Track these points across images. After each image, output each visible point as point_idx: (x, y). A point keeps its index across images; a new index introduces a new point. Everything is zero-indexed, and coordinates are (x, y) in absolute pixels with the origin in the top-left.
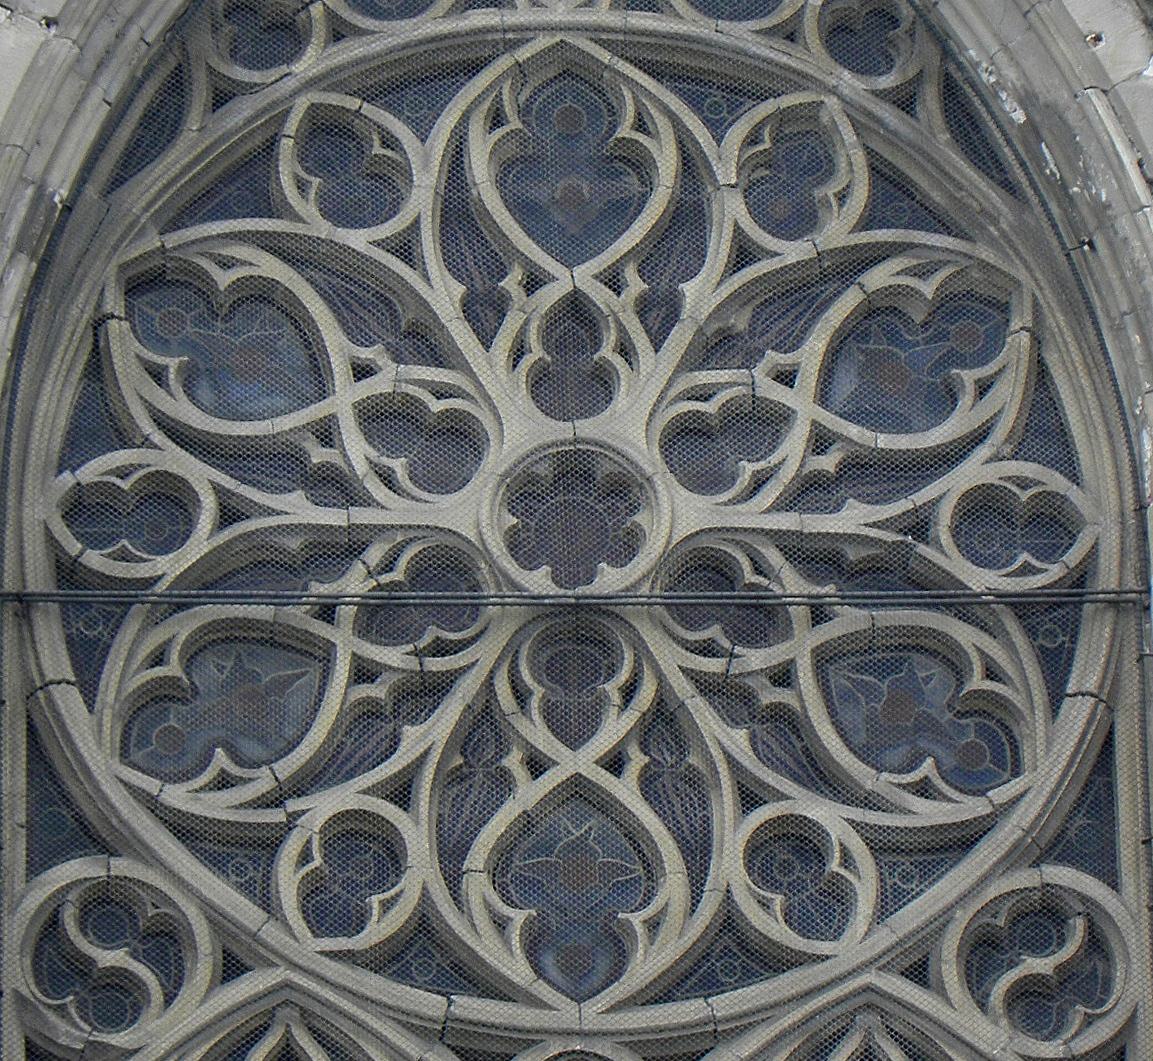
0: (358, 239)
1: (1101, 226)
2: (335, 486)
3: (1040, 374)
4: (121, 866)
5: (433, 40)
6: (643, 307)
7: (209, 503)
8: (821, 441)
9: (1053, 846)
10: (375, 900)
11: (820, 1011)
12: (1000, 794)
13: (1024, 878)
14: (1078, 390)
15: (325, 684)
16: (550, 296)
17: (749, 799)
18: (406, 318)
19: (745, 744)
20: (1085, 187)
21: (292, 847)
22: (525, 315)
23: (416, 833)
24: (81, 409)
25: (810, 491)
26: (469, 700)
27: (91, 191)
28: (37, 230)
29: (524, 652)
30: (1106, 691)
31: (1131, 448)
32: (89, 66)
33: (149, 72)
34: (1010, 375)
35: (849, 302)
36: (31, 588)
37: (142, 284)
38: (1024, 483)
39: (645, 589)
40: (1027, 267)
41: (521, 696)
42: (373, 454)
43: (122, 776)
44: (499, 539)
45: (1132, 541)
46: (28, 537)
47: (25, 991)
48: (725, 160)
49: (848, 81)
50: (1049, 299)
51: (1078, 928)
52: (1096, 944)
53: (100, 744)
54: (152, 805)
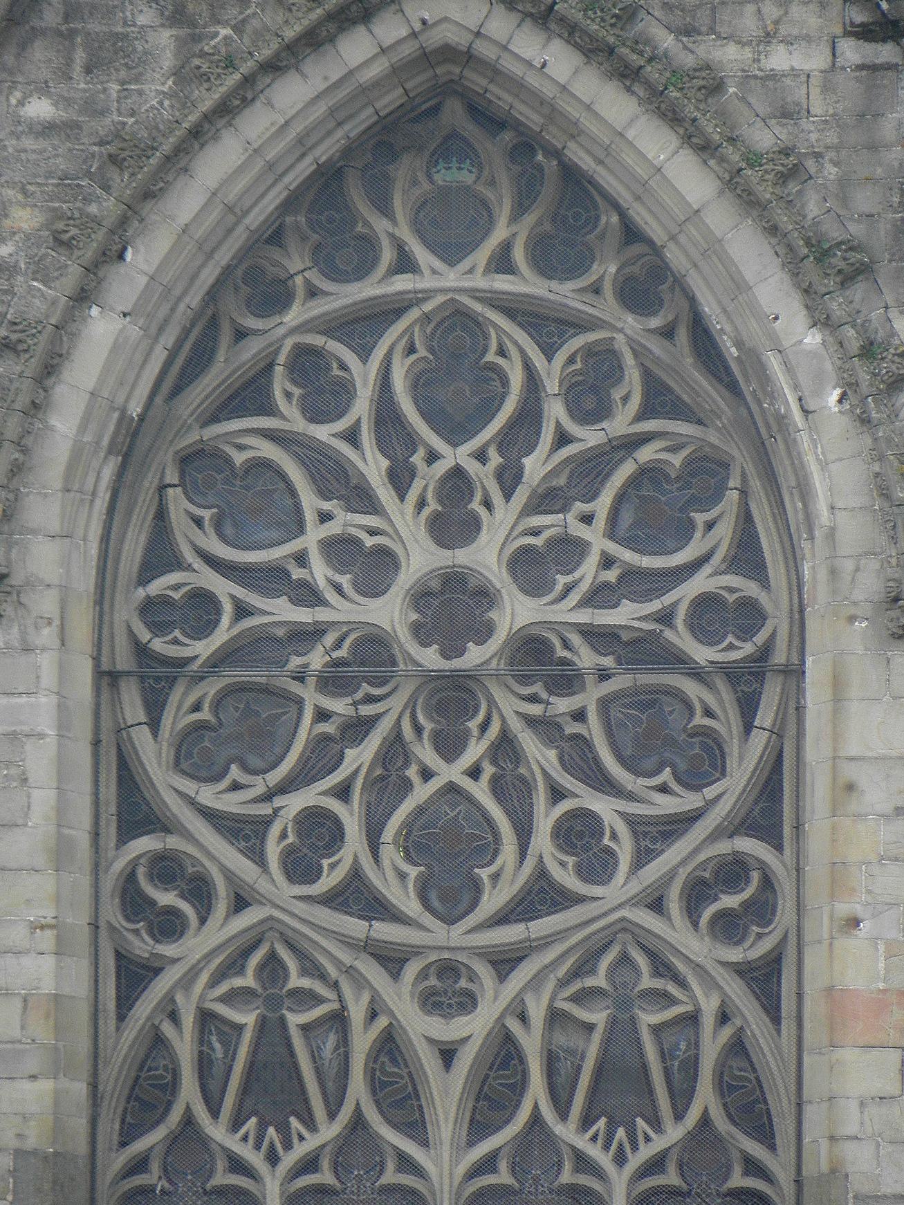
0: (322, 433)
1: (780, 430)
2: (307, 595)
3: (746, 518)
4: (173, 842)
5: (371, 299)
6: (500, 475)
7: (228, 608)
8: (607, 562)
9: (742, 824)
10: (325, 863)
11: (595, 933)
12: (710, 792)
13: (723, 847)
14: (767, 530)
15: (299, 722)
16: (441, 467)
17: (557, 794)
18: (354, 481)
19: (555, 761)
20: (771, 404)
21: (275, 830)
22: (428, 477)
23: (351, 820)
24: (150, 549)
25: (599, 596)
26: (384, 735)
27: (159, 400)
28: (120, 439)
29: (420, 701)
30: (777, 727)
31: (797, 571)
32: (153, 330)
33: (193, 325)
34: (726, 518)
35: (626, 470)
36: (119, 668)
37: (186, 460)
38: (731, 590)
39: (494, 664)
40: (739, 448)
41: (418, 730)
42: (330, 573)
43: (173, 785)
44: (405, 629)
45: (796, 629)
46: (117, 632)
47: (113, 921)
48: (552, 375)
49: (631, 322)
50: (751, 470)
51: (755, 876)
52: (767, 882)
53: (159, 764)
54: (192, 802)
